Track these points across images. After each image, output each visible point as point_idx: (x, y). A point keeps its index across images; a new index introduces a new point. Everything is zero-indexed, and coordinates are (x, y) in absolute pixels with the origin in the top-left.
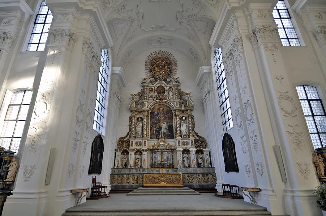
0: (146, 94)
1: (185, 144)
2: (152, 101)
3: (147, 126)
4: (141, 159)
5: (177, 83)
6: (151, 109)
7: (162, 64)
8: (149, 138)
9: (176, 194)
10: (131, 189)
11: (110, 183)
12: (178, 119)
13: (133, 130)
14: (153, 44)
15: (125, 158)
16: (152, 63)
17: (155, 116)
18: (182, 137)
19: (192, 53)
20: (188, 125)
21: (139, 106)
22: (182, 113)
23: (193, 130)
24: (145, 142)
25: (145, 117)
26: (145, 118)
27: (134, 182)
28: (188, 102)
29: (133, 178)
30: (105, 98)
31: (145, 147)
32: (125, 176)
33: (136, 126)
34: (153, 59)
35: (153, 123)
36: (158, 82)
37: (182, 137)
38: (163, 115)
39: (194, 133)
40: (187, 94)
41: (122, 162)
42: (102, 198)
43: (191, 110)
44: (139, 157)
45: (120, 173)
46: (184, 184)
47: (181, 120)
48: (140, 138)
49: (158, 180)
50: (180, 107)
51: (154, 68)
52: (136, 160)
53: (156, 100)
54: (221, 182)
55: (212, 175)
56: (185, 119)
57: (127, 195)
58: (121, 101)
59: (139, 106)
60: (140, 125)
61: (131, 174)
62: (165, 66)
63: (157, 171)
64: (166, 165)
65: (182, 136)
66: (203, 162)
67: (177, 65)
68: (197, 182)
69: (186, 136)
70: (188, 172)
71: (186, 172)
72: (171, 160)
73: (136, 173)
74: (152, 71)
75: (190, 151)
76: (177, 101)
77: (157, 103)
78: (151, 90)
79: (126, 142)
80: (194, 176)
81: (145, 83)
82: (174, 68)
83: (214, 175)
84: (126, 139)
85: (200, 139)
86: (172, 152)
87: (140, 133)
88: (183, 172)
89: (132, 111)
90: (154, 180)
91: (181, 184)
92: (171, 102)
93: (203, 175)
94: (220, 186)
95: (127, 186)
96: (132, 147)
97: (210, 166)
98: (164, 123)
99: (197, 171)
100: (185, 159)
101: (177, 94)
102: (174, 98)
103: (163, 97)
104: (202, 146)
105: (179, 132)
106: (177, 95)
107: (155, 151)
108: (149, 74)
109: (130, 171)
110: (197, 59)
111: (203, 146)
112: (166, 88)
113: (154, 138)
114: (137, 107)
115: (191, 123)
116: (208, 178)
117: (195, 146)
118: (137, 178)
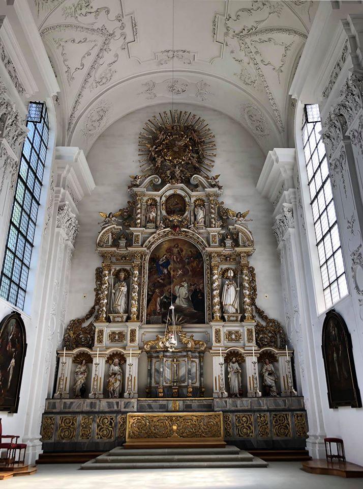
16: (155, 138)
17: (161, 268)
23: (253, 303)
29: (101, 425)
32: (80, 418)
33: (113, 291)
34: (160, 129)
40: (239, 215)
45: (67, 410)
46: (229, 438)
47: (223, 277)
50: (220, 246)
53: (164, 228)
54: (319, 433)
55: (297, 417)
56: (232, 275)
57: (82, 469)
61: (96, 412)
71: (233, 408)
73: (107, 410)
76: (214, 232)
78: (151, 205)
82: (209, 152)
83: (301, 416)
84: (86, 324)
92: (199, 234)
93: (276, 415)
98: (183, 284)
99: (260, 405)
104: (273, 344)
111: (275, 342)
112: (187, 199)
115: (247, 285)
117: (257, 343)
118: (111, 424)
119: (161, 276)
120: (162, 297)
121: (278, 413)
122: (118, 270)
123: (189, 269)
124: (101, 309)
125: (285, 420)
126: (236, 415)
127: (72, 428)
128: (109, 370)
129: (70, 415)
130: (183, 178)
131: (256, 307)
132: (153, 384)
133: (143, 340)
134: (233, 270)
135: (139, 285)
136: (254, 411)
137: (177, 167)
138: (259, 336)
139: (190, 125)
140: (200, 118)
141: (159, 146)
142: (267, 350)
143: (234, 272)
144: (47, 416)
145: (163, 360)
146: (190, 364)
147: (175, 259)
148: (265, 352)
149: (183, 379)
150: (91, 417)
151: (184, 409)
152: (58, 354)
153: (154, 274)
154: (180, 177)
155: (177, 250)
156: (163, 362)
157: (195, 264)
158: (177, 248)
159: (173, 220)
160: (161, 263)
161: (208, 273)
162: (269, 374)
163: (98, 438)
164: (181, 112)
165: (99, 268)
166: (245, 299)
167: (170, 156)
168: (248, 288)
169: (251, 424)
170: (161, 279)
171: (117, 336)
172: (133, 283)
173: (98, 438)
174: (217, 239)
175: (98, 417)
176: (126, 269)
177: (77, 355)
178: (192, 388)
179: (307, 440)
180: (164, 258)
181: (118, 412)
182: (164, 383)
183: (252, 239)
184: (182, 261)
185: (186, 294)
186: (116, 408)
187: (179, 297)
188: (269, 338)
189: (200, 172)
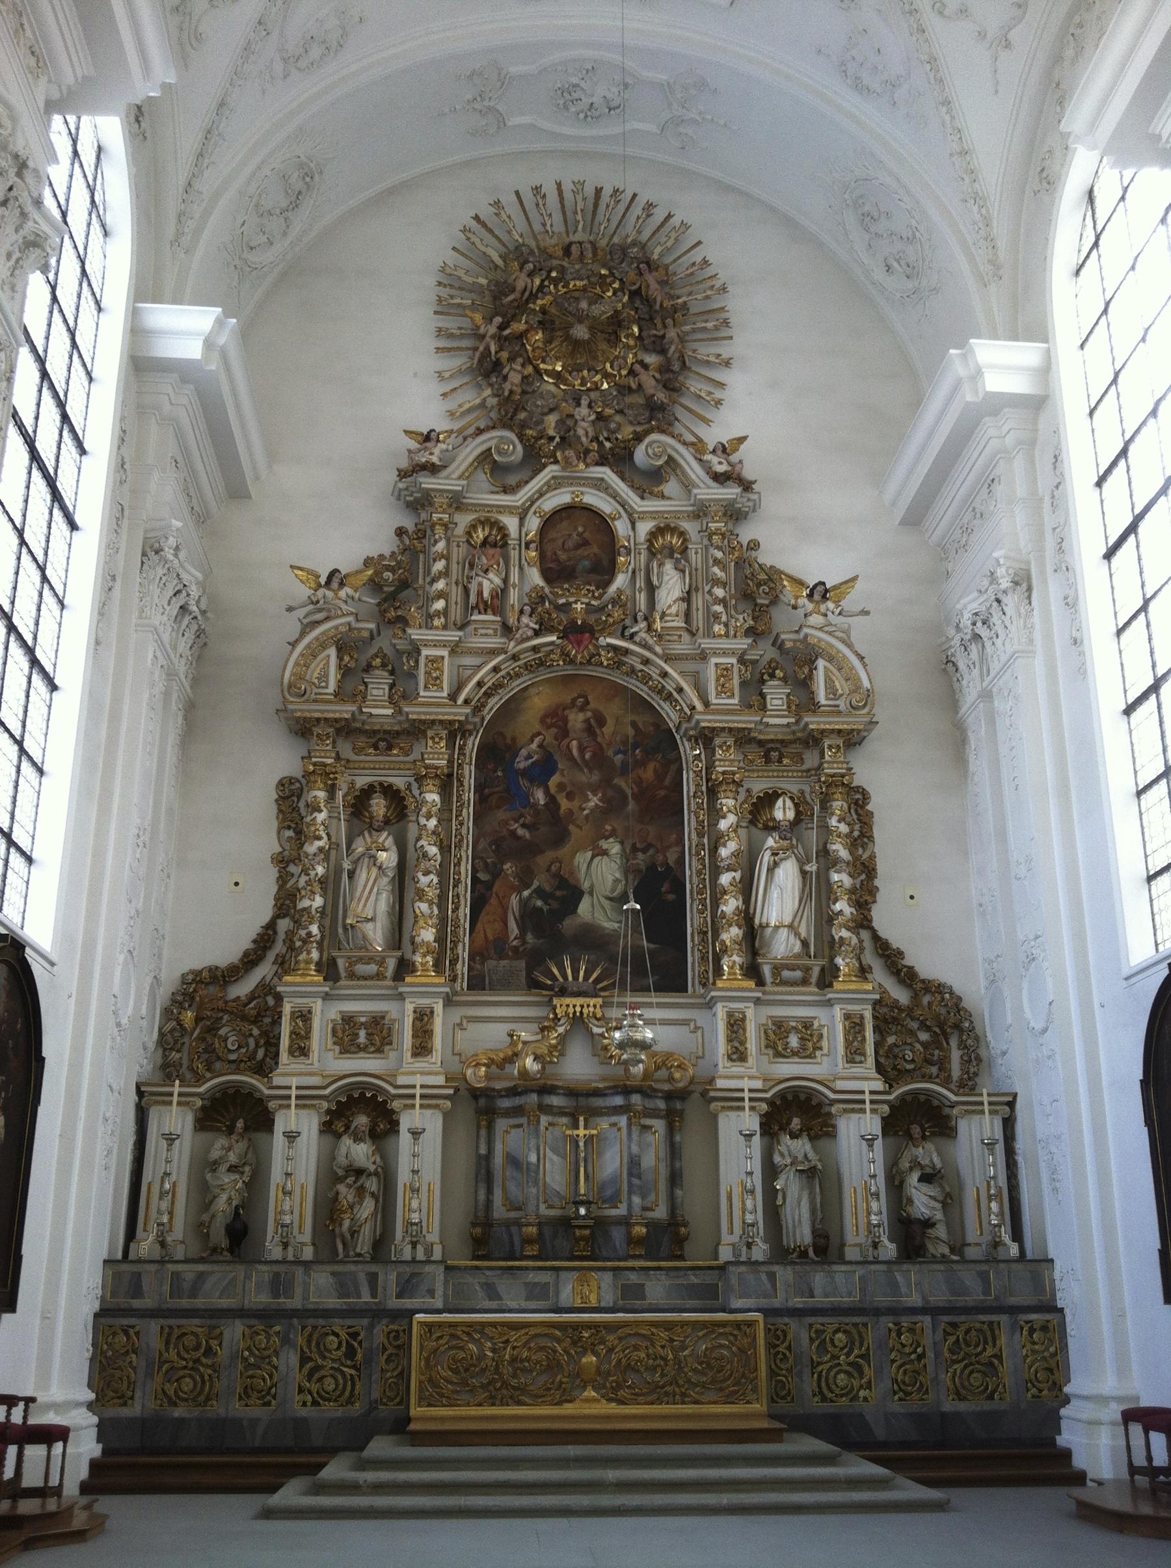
0: (446, 573)
1: (794, 1041)
2: (495, 642)
3: (443, 873)
4: (387, 1177)
5: (731, 492)
6: (488, 714)
7: (596, 310)
8: (462, 983)
9: (725, 1499)
10: (288, 1451)
11: (92, 1396)
12: (731, 819)
13: (319, 901)
14: (514, 121)
15: (232, 1169)
16: (500, 289)
17: (523, 783)
18: (761, 983)
19: (867, 219)
20: (823, 879)
21: (379, 686)
22: (768, 760)
23: (863, 922)
24: (423, 1018)
25: (430, 785)
26: (433, 797)
27: (314, 1387)
28: (821, 663)
29: (315, 1356)
30: (59, 589)
31: (421, 1064)
32: (234, 1331)
33: (347, 865)
34: (518, 255)
35: (497, 842)
36: (551, 471)
37: (761, 983)
38: (595, 777)
39: (868, 944)
40: (821, 593)
41: (203, 1194)
42: (29, 1545)
43: (852, 740)
44: (361, 1152)
45: (185, 1303)
46: (783, 1407)
47: (753, 822)
48: (379, 976)
49: (544, 1378)
50: (746, 705)
51: (521, 336)
52: (340, 1180)
53: (537, 633)
54: (1109, 1385)
55: (1032, 1331)
56: (791, 815)
57: (268, 1514)
58: (200, 633)
59: (379, 686)
60: (382, 856)
61: (294, 1313)
62: (616, 323)
63: (537, 1292)
64: (618, 1234)
65: (767, 970)
66: (945, 1205)
67: (726, 323)
68: (901, 1389)
69: (798, 974)
70: (819, 1300)
71: (798, 1302)
72: (662, 1186)
73: (333, 1302)
74: (497, 365)
75: (833, 1110)
76: (725, 653)
77: (541, 663)
78: (485, 543)
79: (244, 1018)
80: (870, 1338)
81: (432, 469)
82: (705, 350)
83: (1044, 1328)
84: (242, 989)
85: (926, 999)
86: (673, 1119)
87: (376, 935)
88: (777, 1303)
89: (303, 729)
90: (507, 1370)
91: (756, 1407)
92: (667, 659)
93: (954, 1325)
94: (1099, 1423)
95: (254, 1422)
96: (299, 1065)
97: (1014, 1250)
98: (604, 844)
99: (894, 1286)
100: (789, 1184)
101: (724, 585)
102: (699, 619)
103: (601, 609)
104: (934, 1070)
105: (732, 934)
106: (723, 602)
107: (517, 1101)
108: (469, 397)
109: (279, 1285)
110: (910, 285)
111: (943, 1064)
112: (621, 527)
113: (503, 984)
114: (360, 697)
115: (844, 854)
116: (990, 1351)
117: (880, 1068)
118: (351, 1353)
119: (522, 816)
120: (526, 893)
121: (962, 1318)
122: (362, 790)
123: (629, 792)
124: (303, 933)
125: (986, 1342)
126: (811, 1325)
127: (207, 1366)
128: (333, 1158)
129: (197, 1321)
130: (608, 445)
131: (876, 937)
132: (499, 1211)
133: (457, 1049)
134: (792, 798)
135: (445, 849)
136: (877, 1312)
137: (584, 402)
138: (883, 1039)
139: (634, 243)
140: (669, 216)
141: (514, 318)
142: (915, 1093)
143: (796, 805)
144: (110, 1321)
145: (538, 1122)
146: (635, 1136)
147: (575, 752)
148: (909, 1098)
149: (609, 1192)
150: (277, 1328)
151: (615, 1303)
152: (140, 1093)
153: (499, 807)
154: (596, 439)
155: (581, 717)
156: (537, 1131)
157: (648, 773)
158: (582, 709)
159: (569, 604)
160: (522, 765)
161: (700, 806)
162: (922, 1179)
163: (304, 1404)
164: (598, 191)
165: (291, 780)
166: (838, 907)
167: (557, 359)
168: (848, 863)
169: (865, 1357)
170: (524, 826)
171: (362, 1033)
172: (418, 839)
173: (304, 1404)
174: (736, 681)
175: (303, 1328)
176: (390, 786)
177: (213, 1100)
178: (647, 1225)
179: (1063, 1412)
180: (534, 746)
181: (377, 1313)
182: (542, 1207)
183: (866, 683)
184: (600, 760)
185: (616, 881)
186: (366, 1298)
187: (591, 893)
188: (918, 1046)
189: (670, 424)
